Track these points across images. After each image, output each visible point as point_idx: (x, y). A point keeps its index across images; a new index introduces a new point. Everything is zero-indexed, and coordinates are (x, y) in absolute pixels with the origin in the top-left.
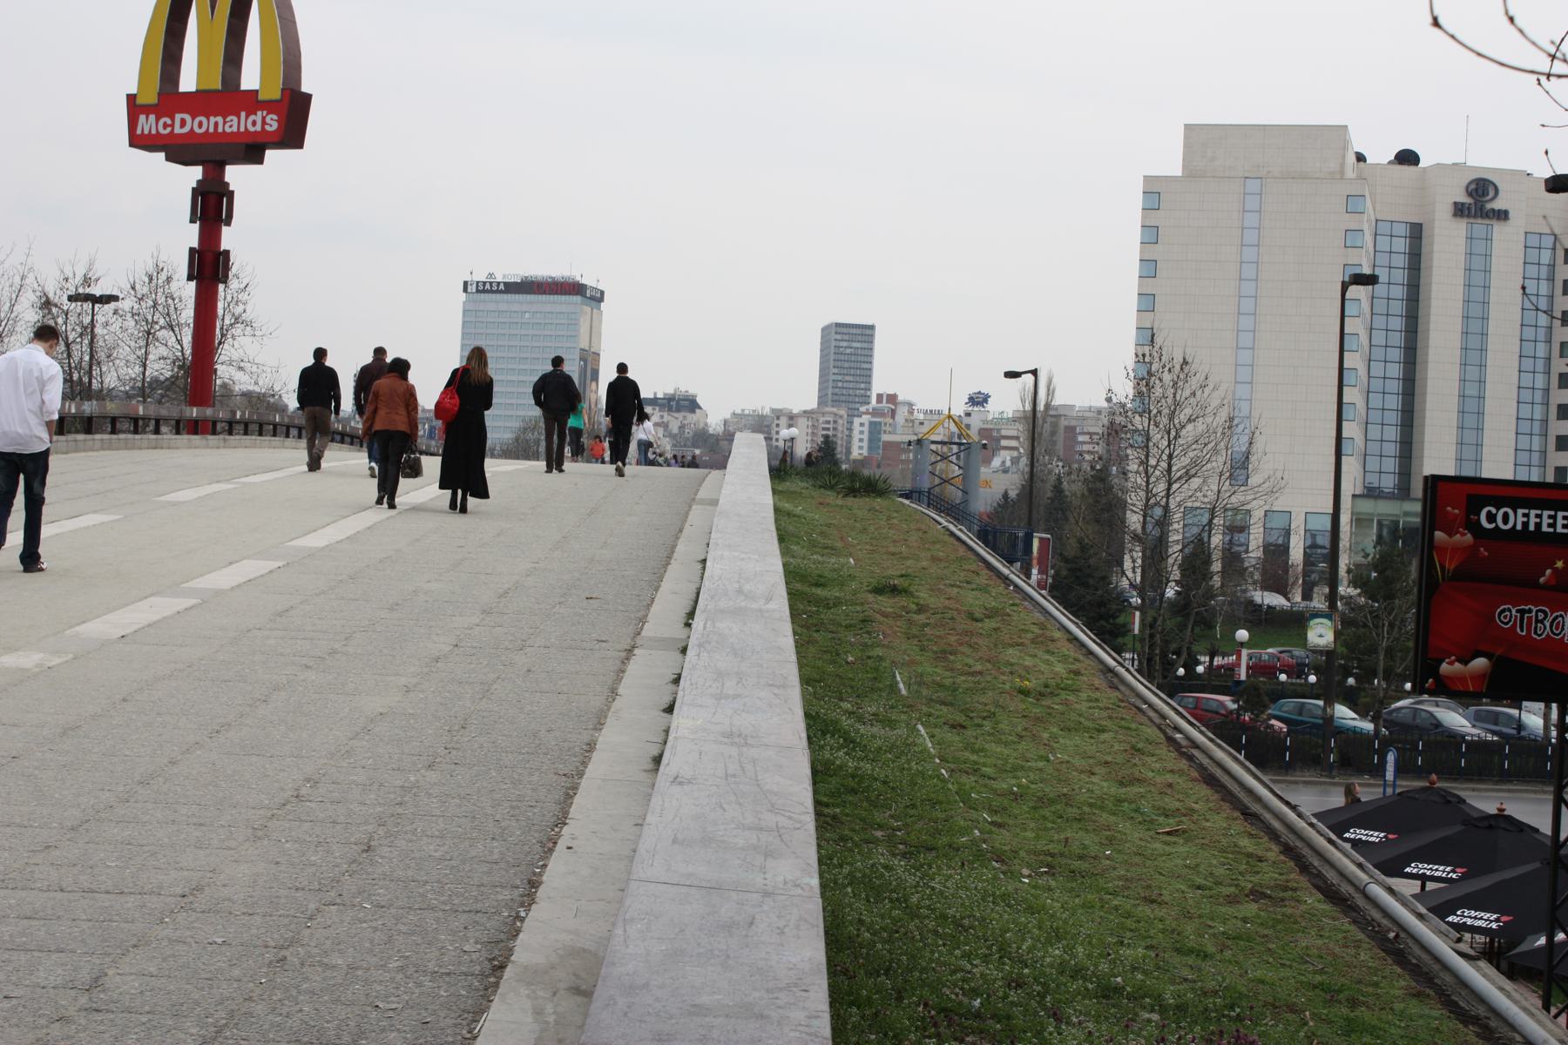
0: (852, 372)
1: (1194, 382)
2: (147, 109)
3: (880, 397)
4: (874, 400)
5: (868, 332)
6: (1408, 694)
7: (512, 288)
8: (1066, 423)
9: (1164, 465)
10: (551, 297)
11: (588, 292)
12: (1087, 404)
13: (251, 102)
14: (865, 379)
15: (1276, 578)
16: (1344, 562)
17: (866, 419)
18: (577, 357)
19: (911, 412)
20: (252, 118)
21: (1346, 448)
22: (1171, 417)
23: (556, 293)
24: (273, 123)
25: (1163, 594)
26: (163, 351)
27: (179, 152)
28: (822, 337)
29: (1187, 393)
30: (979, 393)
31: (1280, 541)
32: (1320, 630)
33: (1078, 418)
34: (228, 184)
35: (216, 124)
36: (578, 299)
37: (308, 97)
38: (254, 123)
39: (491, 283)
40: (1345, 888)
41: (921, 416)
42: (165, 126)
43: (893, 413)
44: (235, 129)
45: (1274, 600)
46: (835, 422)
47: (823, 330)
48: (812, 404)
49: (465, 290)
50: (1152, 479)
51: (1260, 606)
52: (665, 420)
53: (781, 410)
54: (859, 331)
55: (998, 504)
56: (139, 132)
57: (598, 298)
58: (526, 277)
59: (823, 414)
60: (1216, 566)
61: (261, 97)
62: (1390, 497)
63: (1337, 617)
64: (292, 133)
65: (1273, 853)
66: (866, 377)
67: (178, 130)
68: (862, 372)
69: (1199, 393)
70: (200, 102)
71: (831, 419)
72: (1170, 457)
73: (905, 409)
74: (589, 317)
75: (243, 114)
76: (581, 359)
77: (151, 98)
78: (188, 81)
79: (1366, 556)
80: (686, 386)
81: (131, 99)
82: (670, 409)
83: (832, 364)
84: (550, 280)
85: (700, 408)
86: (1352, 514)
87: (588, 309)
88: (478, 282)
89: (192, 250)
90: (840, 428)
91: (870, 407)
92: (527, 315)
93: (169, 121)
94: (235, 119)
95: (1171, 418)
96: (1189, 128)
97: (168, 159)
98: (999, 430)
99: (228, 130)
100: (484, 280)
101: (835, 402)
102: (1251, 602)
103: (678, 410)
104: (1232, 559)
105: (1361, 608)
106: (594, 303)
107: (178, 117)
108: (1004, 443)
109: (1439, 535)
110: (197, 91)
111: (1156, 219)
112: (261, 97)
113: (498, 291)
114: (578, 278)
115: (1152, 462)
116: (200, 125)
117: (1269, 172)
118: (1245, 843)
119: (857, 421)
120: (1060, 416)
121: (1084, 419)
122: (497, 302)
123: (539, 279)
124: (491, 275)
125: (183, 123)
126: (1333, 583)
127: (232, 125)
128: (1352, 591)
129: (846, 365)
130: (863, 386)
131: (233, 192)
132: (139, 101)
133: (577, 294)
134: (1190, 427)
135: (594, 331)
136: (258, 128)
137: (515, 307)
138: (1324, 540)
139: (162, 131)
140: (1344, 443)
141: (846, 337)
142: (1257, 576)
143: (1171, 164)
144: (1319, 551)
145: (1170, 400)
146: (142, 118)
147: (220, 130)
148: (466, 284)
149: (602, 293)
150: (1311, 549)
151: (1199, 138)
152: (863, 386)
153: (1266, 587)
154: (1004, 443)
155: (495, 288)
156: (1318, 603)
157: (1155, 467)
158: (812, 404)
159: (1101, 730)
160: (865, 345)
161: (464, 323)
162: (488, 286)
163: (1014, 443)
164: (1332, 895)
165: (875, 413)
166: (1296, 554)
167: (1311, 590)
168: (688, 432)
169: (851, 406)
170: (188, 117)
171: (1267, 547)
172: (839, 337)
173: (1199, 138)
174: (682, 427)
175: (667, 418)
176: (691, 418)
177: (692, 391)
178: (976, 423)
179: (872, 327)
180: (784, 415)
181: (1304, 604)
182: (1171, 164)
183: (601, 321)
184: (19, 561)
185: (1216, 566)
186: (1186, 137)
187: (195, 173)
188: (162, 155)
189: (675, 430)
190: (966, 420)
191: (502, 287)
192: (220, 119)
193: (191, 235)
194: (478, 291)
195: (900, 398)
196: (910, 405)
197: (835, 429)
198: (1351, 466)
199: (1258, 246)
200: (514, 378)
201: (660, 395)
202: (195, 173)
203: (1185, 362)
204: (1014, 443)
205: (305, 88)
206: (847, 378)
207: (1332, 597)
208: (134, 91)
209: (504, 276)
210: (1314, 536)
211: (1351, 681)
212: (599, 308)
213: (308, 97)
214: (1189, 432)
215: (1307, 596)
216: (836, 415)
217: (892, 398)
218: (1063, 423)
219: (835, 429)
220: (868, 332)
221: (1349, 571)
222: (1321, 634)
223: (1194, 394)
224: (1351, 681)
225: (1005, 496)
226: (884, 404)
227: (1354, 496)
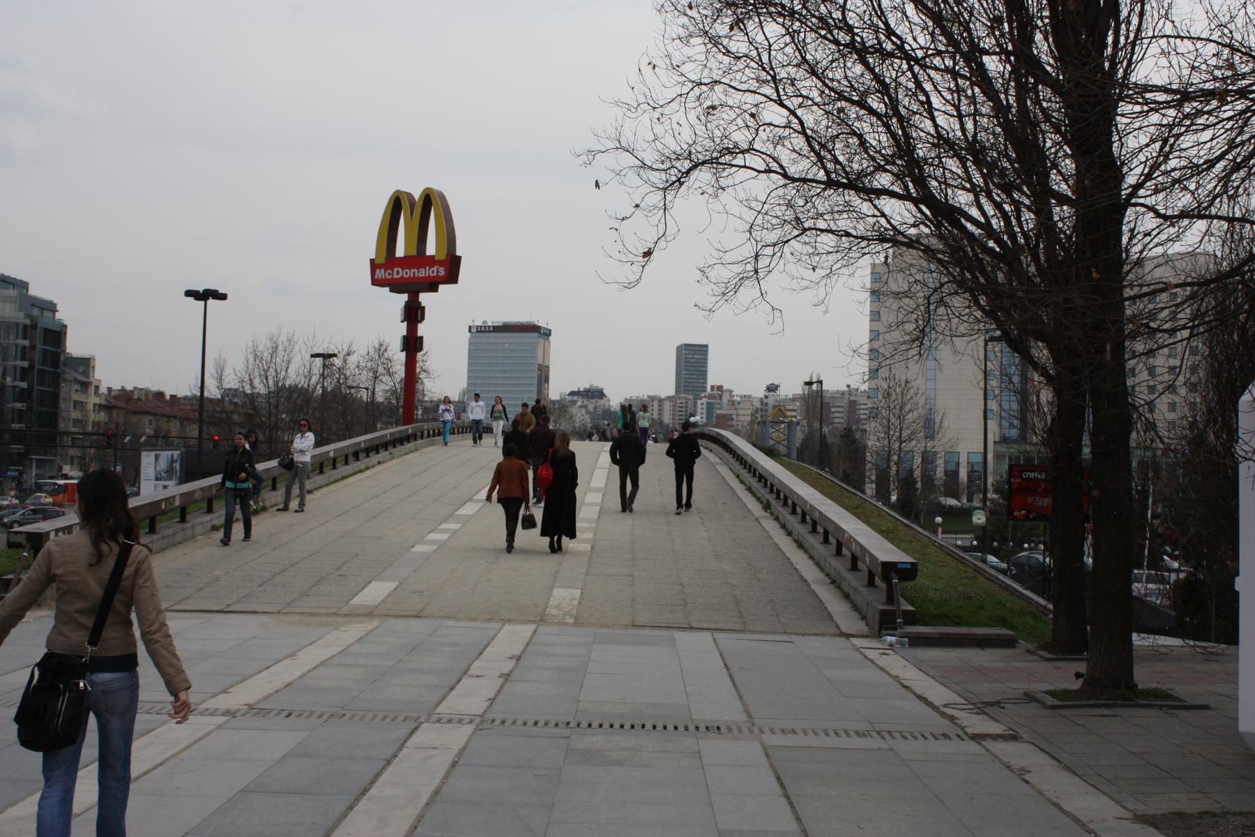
0: (695, 372)
1: (912, 392)
2: (381, 266)
3: (712, 387)
4: (709, 389)
5: (703, 349)
6: (1026, 550)
9: (898, 434)
10: (520, 334)
12: (836, 389)
13: (431, 261)
15: (954, 493)
16: (990, 480)
17: (704, 400)
18: (537, 369)
19: (732, 396)
20: (432, 269)
21: (990, 415)
22: (901, 409)
23: (516, 332)
24: (442, 272)
25: (890, 499)
26: (383, 387)
27: (396, 287)
28: (677, 352)
29: (908, 397)
31: (953, 469)
32: (979, 516)
33: (830, 398)
34: (420, 303)
35: (414, 273)
36: (536, 335)
37: (460, 258)
38: (433, 272)
40: (992, 578)
41: (739, 399)
42: (389, 274)
43: (721, 397)
44: (423, 275)
45: (952, 502)
46: (686, 403)
47: (677, 348)
48: (672, 392)
49: (470, 331)
50: (892, 442)
52: (585, 403)
53: (653, 397)
54: (699, 348)
56: (376, 277)
57: (547, 334)
59: (679, 398)
60: (919, 485)
61: (436, 259)
62: (1015, 441)
63: (987, 509)
64: (452, 276)
65: (971, 570)
66: (703, 375)
67: (395, 276)
69: (914, 397)
70: (406, 262)
71: (684, 401)
72: (901, 430)
73: (728, 394)
75: (427, 268)
76: (539, 370)
77: (382, 260)
78: (400, 252)
79: (1002, 477)
80: (598, 384)
81: (372, 261)
82: (588, 398)
83: (683, 368)
85: (606, 396)
86: (994, 452)
87: (542, 341)
89: (404, 336)
90: (689, 406)
91: (707, 394)
93: (391, 272)
94: (423, 270)
95: (901, 410)
97: (391, 291)
98: (785, 406)
99: (420, 276)
101: (686, 391)
102: (939, 504)
103: (593, 398)
104: (928, 479)
105: (999, 504)
106: (545, 337)
107: (395, 270)
109: (1013, 480)
110: (405, 257)
112: (436, 259)
113: (489, 331)
114: (536, 323)
115: (892, 433)
116: (406, 274)
118: (962, 568)
119: (699, 402)
121: (834, 398)
122: (488, 337)
124: (485, 322)
125: (398, 273)
126: (985, 492)
127: (422, 273)
128: (995, 496)
129: (692, 368)
130: (702, 381)
131: (424, 307)
132: (376, 262)
133: (535, 332)
134: (910, 415)
135: (546, 353)
136: (435, 274)
137: (499, 341)
138: (979, 468)
139: (388, 277)
140: (989, 413)
141: (691, 352)
142: (942, 490)
144: (976, 474)
145: (900, 401)
146: (378, 271)
148: (470, 327)
149: (550, 331)
150: (971, 473)
152: (702, 381)
153: (947, 495)
156: (976, 503)
157: (893, 436)
158: (672, 392)
159: (912, 542)
160: (703, 357)
161: (469, 350)
162: (483, 329)
163: (794, 414)
164: (988, 579)
165: (710, 397)
166: (963, 474)
167: (972, 496)
168: (599, 411)
169: (695, 393)
170: (400, 270)
171: (946, 473)
172: (687, 352)
174: (595, 408)
175: (586, 402)
176: (601, 402)
177: (600, 386)
178: (771, 401)
179: (706, 346)
180: (656, 399)
181: (968, 504)
183: (549, 347)
185: (919, 485)
187: (404, 297)
188: (388, 289)
189: (592, 410)
190: (765, 401)
191: (491, 329)
192: (416, 270)
193: (402, 329)
194: (477, 331)
195: (725, 388)
196: (731, 391)
197: (686, 407)
198: (993, 426)
200: (500, 382)
201: (582, 389)
202: (404, 297)
203: (907, 382)
204: (794, 414)
205: (458, 254)
206: (693, 377)
207: (985, 500)
208: (373, 257)
209: (493, 322)
210: (972, 466)
211: (995, 544)
212: (548, 340)
213: (460, 258)
214: (910, 417)
215: (970, 500)
216: (686, 398)
217: (720, 388)
219: (686, 407)
220: (703, 349)
221: (993, 485)
222: (979, 518)
223: (912, 398)
224: (995, 544)
226: (715, 392)
227: (995, 442)
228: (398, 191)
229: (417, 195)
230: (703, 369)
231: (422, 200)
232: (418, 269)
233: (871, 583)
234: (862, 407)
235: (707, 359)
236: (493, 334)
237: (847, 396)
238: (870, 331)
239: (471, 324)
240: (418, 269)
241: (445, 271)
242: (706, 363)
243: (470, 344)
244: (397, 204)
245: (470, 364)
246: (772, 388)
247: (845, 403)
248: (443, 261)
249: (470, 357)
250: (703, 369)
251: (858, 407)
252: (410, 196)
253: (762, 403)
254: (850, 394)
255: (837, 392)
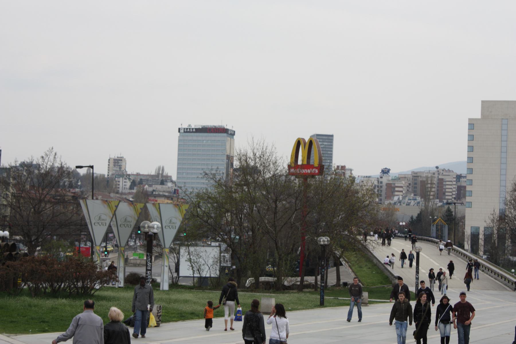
2: (292, 168)
5: (330, 138)
7: (198, 130)
8: (421, 179)
11: (229, 132)
14: (329, 158)
23: (212, 132)
24: (317, 171)
30: (386, 168)
36: (225, 135)
39: (190, 129)
49: (179, 131)
51: (513, 261)
55: (409, 221)
57: (233, 134)
58: (204, 126)
68: (328, 155)
70: (303, 166)
74: (229, 142)
78: (300, 162)
84: (214, 127)
87: (229, 139)
88: (184, 129)
92: (205, 141)
96: (483, 102)
98: (394, 184)
100: (187, 127)
102: (509, 260)
108: (397, 189)
111: (473, 132)
113: (193, 132)
117: (510, 116)
120: (418, 176)
123: (210, 127)
124: (190, 125)
130: (329, 161)
133: (225, 133)
137: (200, 138)
143: (477, 115)
147: (306, 172)
148: (179, 129)
149: (234, 132)
151: (486, 105)
152: (329, 161)
154: (397, 189)
155: (191, 131)
160: (329, 144)
161: (179, 145)
162: (188, 130)
163: (401, 189)
173: (486, 105)
178: (385, 180)
179: (332, 136)
182: (477, 115)
183: (234, 144)
184: (455, 268)
186: (482, 105)
190: (380, 180)
191: (194, 130)
192: (306, 170)
194: (184, 132)
195: (347, 167)
199: (507, 141)
204: (401, 189)
209: (195, 126)
212: (233, 138)
218: (420, 179)
220: (330, 138)
225: (412, 218)
228: (299, 138)
229: (307, 140)
230: (329, 152)
231: (309, 142)
232: (307, 170)
233: (512, 284)
234: (447, 183)
235: (332, 145)
236: (196, 134)
237: (436, 175)
238: (468, 146)
239: (180, 127)
240: (307, 170)
241: (318, 171)
242: (332, 148)
243: (180, 141)
244: (298, 143)
245: (179, 155)
246: (385, 171)
247: (435, 181)
248: (317, 167)
249: (179, 150)
250: (329, 152)
251: (444, 183)
252: (303, 139)
253: (378, 181)
254: (439, 174)
255: (429, 172)
